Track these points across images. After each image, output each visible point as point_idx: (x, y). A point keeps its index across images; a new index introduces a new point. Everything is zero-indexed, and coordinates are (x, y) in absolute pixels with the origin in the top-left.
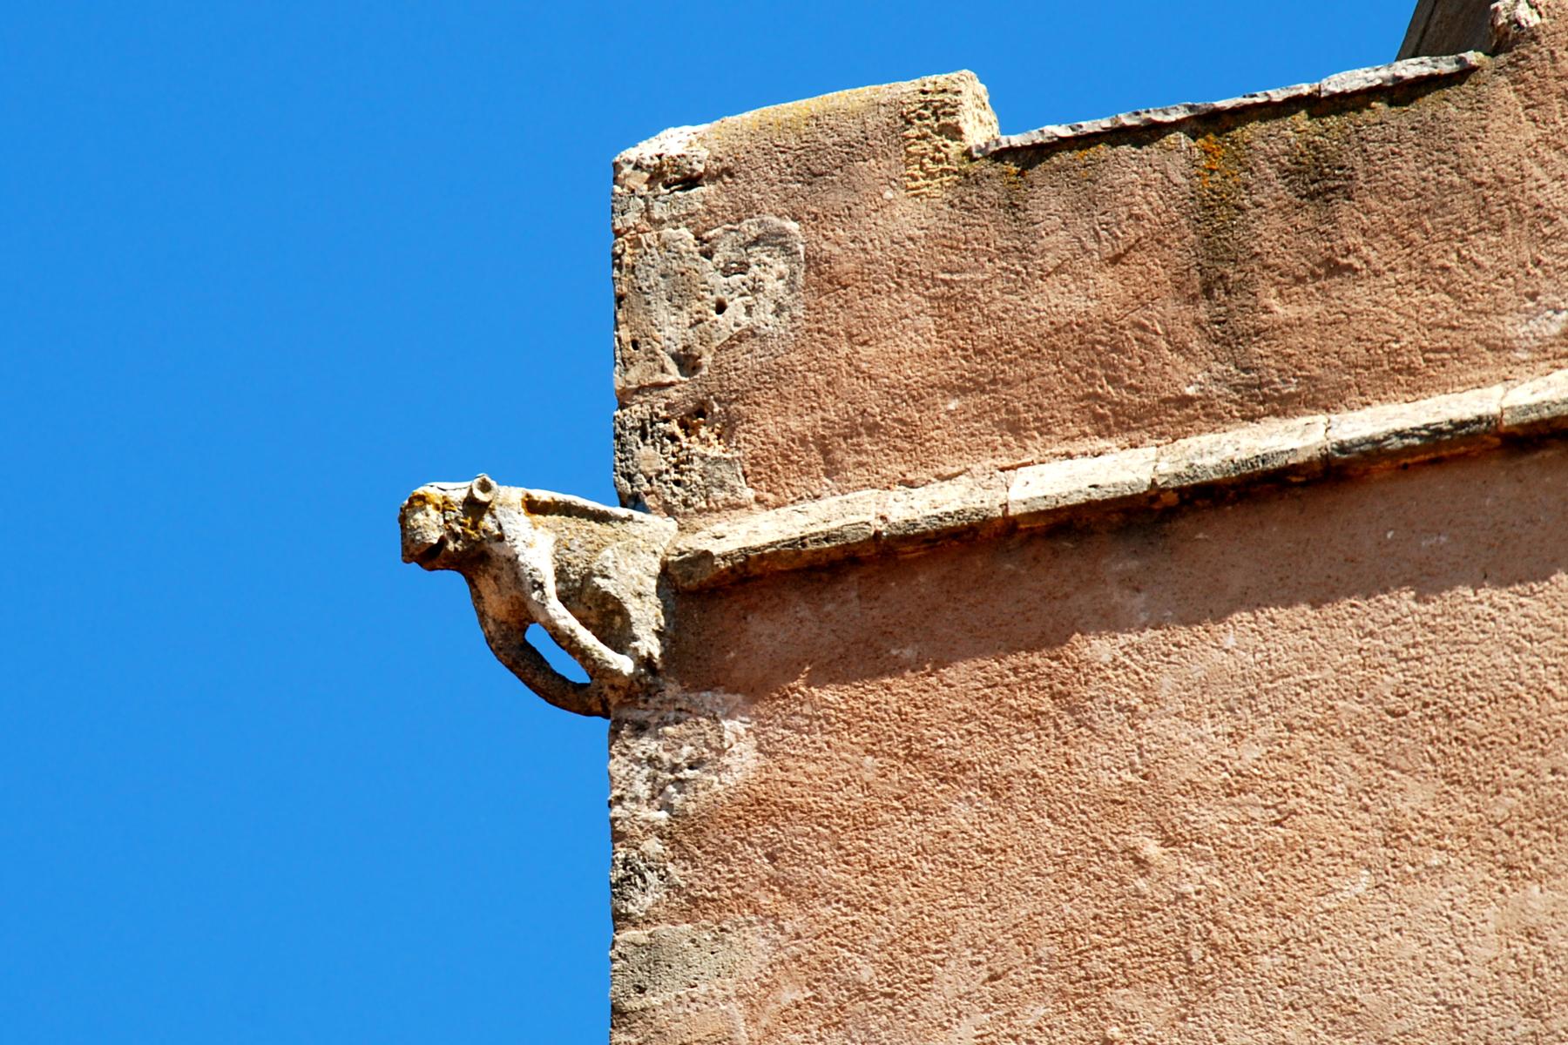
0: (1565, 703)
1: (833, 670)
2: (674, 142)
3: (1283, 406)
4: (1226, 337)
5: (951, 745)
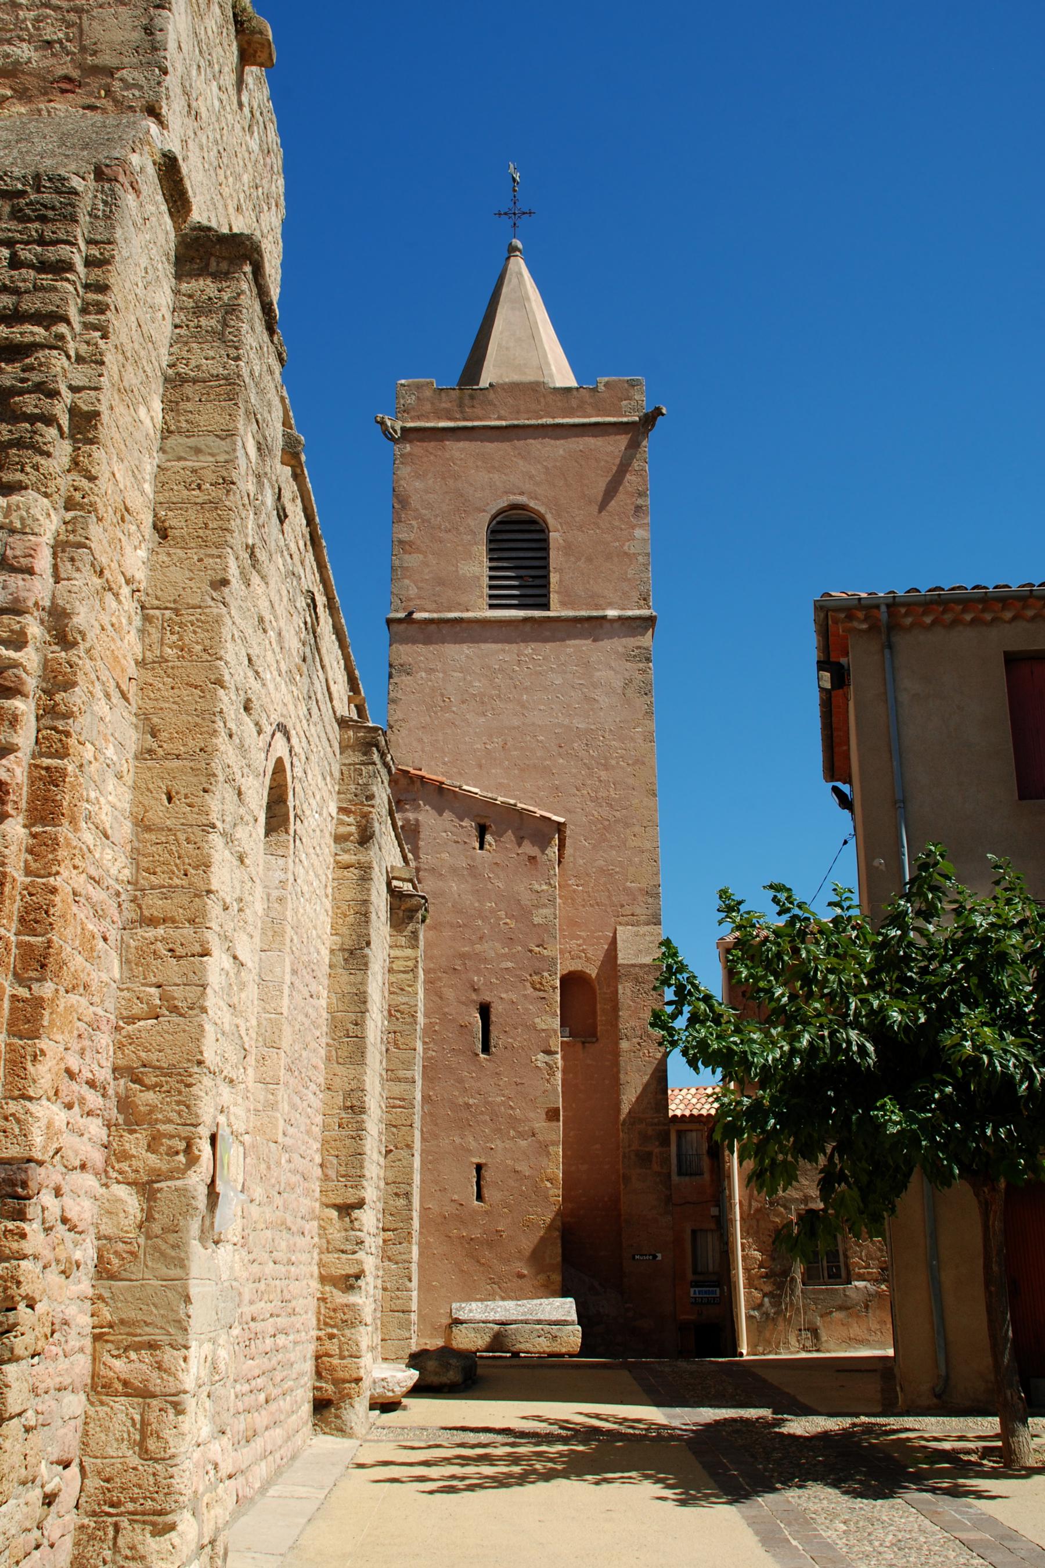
0: (6, 437)
1: (419, 441)
2: (403, 381)
3: (468, 420)
4: (462, 412)
5: (430, 450)
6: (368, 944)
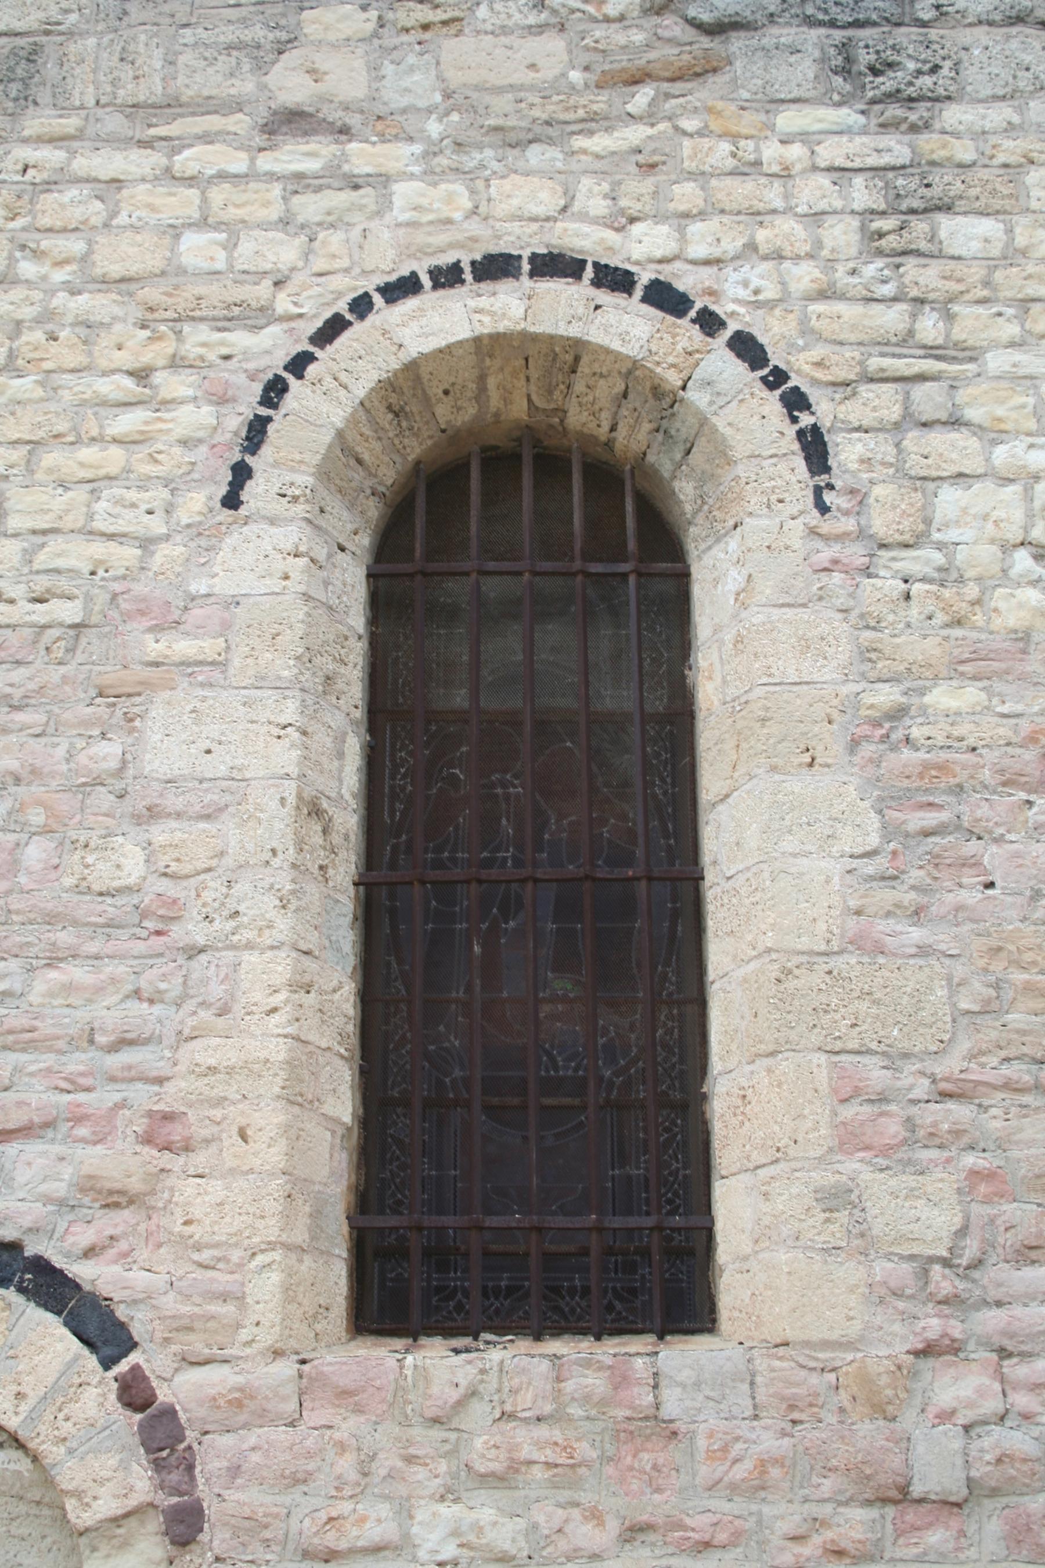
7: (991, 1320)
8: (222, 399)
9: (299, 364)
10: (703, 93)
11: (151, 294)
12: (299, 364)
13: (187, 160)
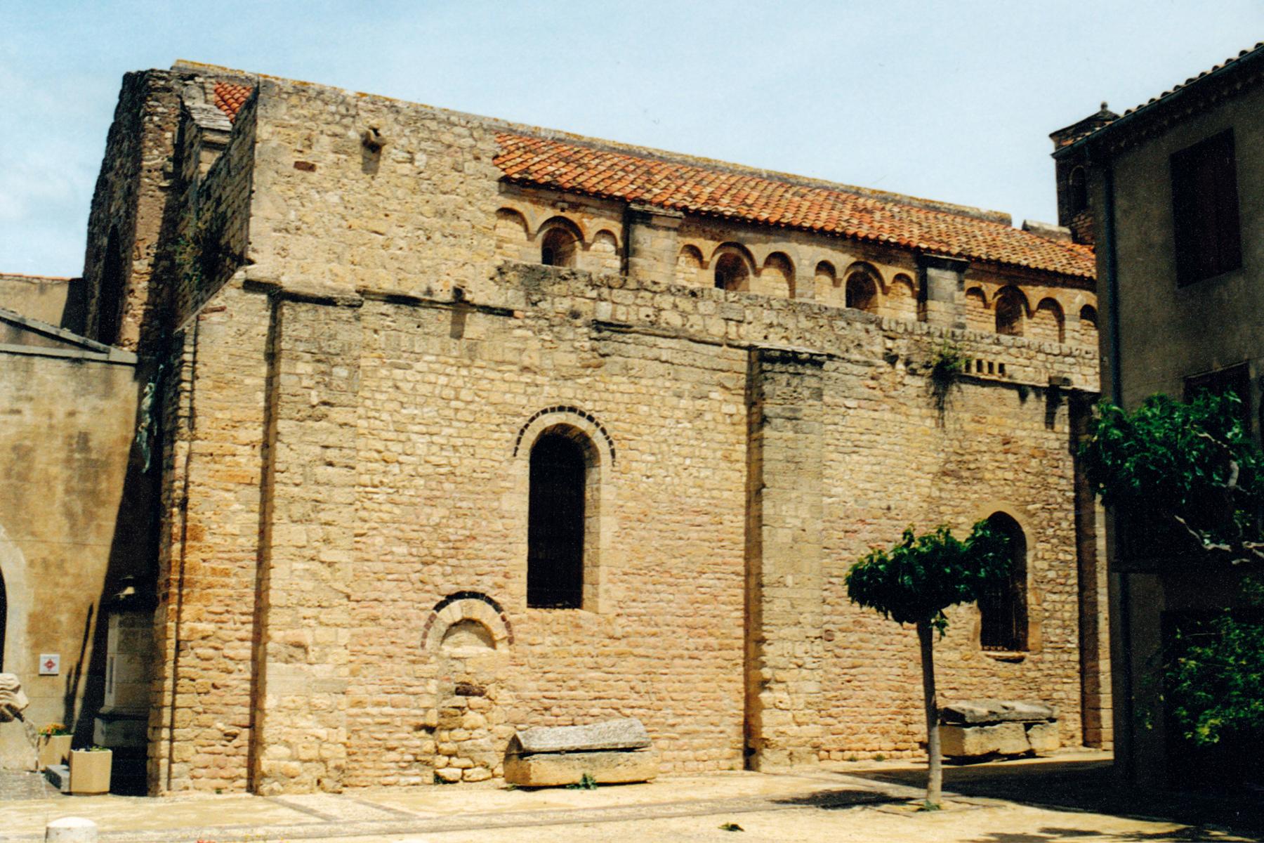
6: (764, 486)
7: (627, 611)
8: (512, 433)
9: (526, 426)
10: (599, 371)
11: (500, 407)
12: (526, 426)
13: (507, 376)
